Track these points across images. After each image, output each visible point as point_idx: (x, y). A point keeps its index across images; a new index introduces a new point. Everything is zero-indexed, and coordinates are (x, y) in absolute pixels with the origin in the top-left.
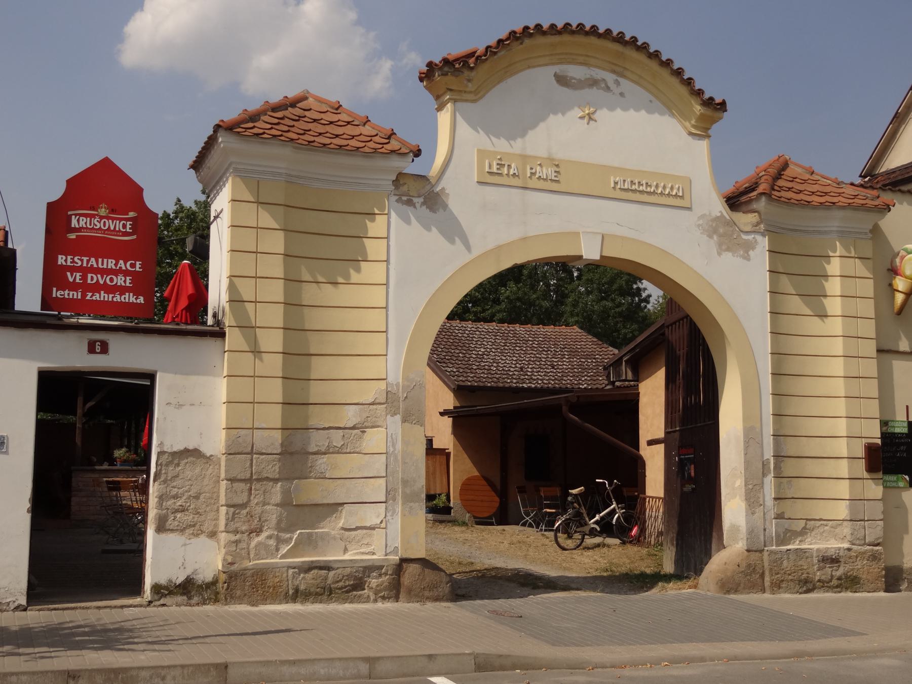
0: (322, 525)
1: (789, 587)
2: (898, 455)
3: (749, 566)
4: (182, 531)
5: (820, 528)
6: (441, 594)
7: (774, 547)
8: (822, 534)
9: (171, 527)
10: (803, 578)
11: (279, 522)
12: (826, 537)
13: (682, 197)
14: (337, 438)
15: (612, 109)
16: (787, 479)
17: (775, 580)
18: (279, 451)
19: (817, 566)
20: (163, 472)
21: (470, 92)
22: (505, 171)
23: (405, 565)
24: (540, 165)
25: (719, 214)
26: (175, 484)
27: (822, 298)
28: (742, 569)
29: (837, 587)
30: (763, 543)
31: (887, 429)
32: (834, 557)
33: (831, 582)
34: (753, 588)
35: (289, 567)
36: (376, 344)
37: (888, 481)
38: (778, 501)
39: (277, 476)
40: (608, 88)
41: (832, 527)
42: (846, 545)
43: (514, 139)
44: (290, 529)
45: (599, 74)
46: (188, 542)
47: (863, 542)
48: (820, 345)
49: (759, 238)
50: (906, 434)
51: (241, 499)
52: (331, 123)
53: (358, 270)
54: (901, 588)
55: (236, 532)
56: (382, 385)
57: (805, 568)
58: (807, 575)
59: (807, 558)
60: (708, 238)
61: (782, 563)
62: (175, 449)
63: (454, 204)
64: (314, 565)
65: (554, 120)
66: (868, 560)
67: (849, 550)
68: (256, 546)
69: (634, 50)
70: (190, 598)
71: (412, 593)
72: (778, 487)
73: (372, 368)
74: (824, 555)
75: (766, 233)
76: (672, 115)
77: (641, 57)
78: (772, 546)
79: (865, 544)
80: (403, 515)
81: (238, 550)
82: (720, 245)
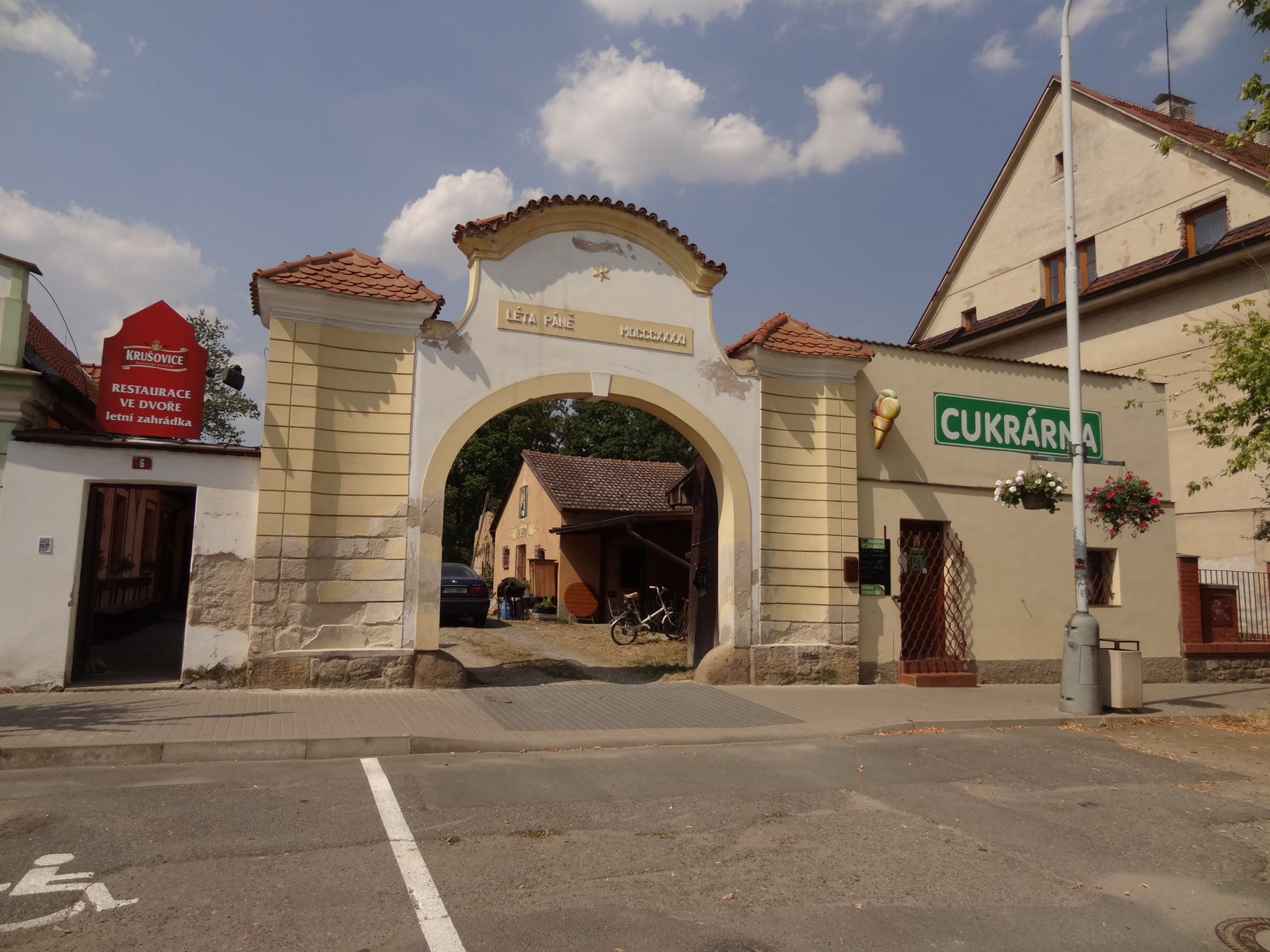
3: (736, 661)
4: (216, 623)
8: (804, 634)
9: (205, 620)
11: (303, 618)
13: (685, 345)
14: (363, 546)
15: (624, 269)
18: (306, 556)
20: (199, 572)
21: (495, 252)
22: (524, 319)
23: (419, 656)
25: (718, 361)
26: (210, 583)
29: (815, 679)
35: (311, 657)
36: (400, 464)
38: (765, 606)
39: (303, 578)
40: (621, 252)
42: (825, 644)
43: (534, 292)
44: (314, 623)
46: (220, 633)
49: (753, 381)
50: (883, 550)
53: (387, 402)
55: (263, 625)
56: (404, 501)
62: (211, 553)
63: (476, 347)
66: (844, 657)
67: (828, 648)
68: (281, 638)
72: (765, 594)
73: (397, 485)
75: (760, 377)
76: (679, 276)
79: (842, 643)
80: (419, 613)
81: (263, 641)
82: (718, 386)
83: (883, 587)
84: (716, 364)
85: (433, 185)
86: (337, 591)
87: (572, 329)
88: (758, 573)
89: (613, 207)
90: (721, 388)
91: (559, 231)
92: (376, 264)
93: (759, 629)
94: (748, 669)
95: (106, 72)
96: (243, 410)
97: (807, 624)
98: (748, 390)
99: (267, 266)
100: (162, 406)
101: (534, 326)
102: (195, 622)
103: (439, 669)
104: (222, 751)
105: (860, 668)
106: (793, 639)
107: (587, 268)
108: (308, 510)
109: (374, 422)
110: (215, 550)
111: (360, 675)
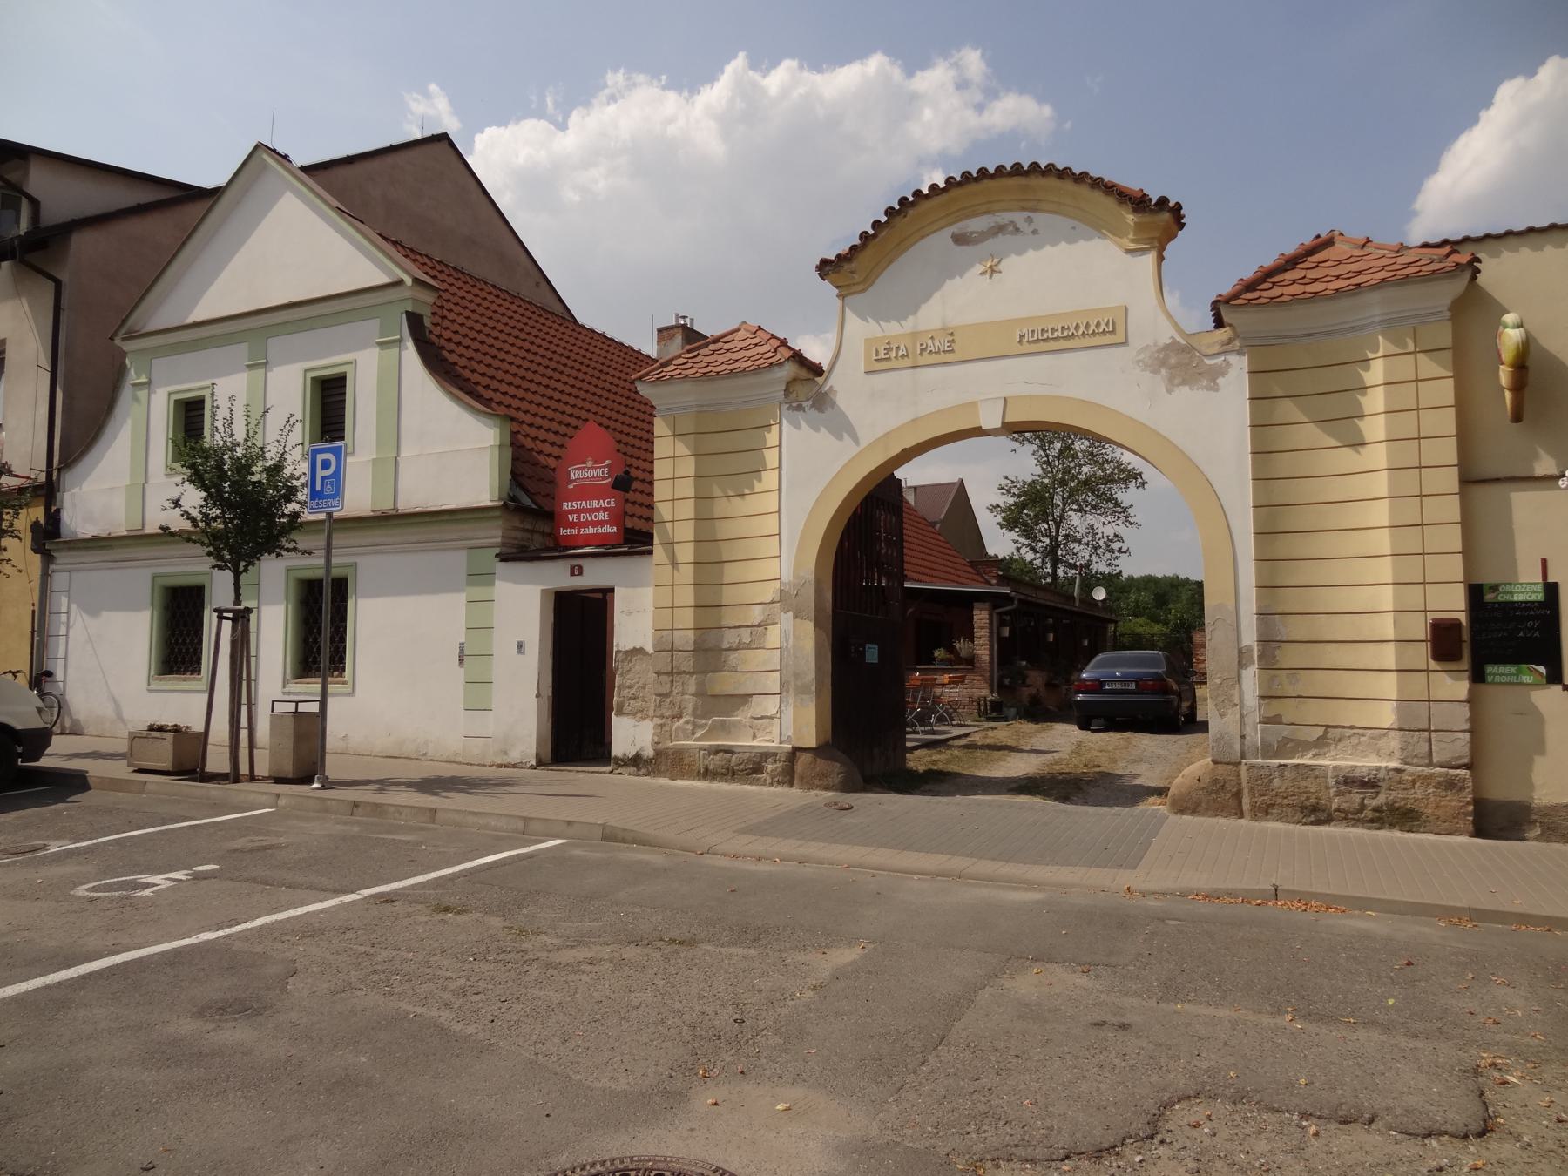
0: (736, 713)
1: (1284, 814)
2: (1521, 634)
3: (1215, 781)
4: (634, 714)
5: (1352, 738)
6: (831, 784)
7: (1259, 760)
8: (1355, 747)
9: (627, 712)
10: (1308, 804)
11: (694, 710)
12: (1362, 751)
13: (1113, 332)
14: (746, 635)
15: (1020, 252)
16: (1288, 671)
17: (1258, 803)
19: (1335, 789)
21: (858, 284)
22: (893, 354)
23: (798, 753)
24: (932, 338)
25: (1169, 341)
27: (1356, 420)
28: (1202, 785)
29: (1372, 821)
30: (1239, 755)
31: (1497, 596)
32: (1366, 779)
33: (1362, 813)
34: (1222, 811)
35: (700, 749)
37: (1498, 674)
38: (1267, 701)
39: (692, 670)
40: (1017, 230)
41: (1372, 738)
42: (1394, 764)
43: (905, 318)
44: (705, 716)
45: (1004, 218)
46: (637, 723)
47: (1427, 761)
48: (1355, 487)
49: (1233, 359)
50: (1539, 602)
51: (666, 688)
52: (741, 349)
53: (760, 480)
54: (1526, 835)
55: (662, 717)
57: (1312, 790)
58: (1316, 801)
59: (1316, 777)
60: (1151, 375)
61: (1271, 781)
62: (627, 649)
63: (842, 400)
64: (722, 748)
65: (953, 286)
66: (1437, 788)
67: (1398, 771)
68: (676, 729)
69: (1041, 177)
70: (638, 770)
71: (805, 780)
73: (770, 569)
74: (1347, 775)
75: (1245, 349)
76: (1105, 237)
77: (1052, 182)
78: (1258, 758)
79: (1431, 764)
80: (795, 706)
82: (1171, 380)
83: (1542, 669)
84: (1166, 347)
85: (1487, 102)
86: (725, 683)
87: (952, 351)
88: (1252, 650)
89: (992, 177)
90: (1176, 381)
91: (935, 231)
92: (754, 334)
93: (1255, 736)
94: (1238, 795)
95: (1068, 125)
96: (1126, 481)
97: (1361, 731)
98: (1223, 374)
99: (1226, 289)
100: (596, 517)
101: (906, 358)
102: (620, 713)
103: (818, 769)
104: (471, 819)
105: (1475, 809)
106: (1333, 753)
107: (972, 265)
108: (692, 603)
109: (751, 504)
110: (629, 647)
111: (742, 771)
